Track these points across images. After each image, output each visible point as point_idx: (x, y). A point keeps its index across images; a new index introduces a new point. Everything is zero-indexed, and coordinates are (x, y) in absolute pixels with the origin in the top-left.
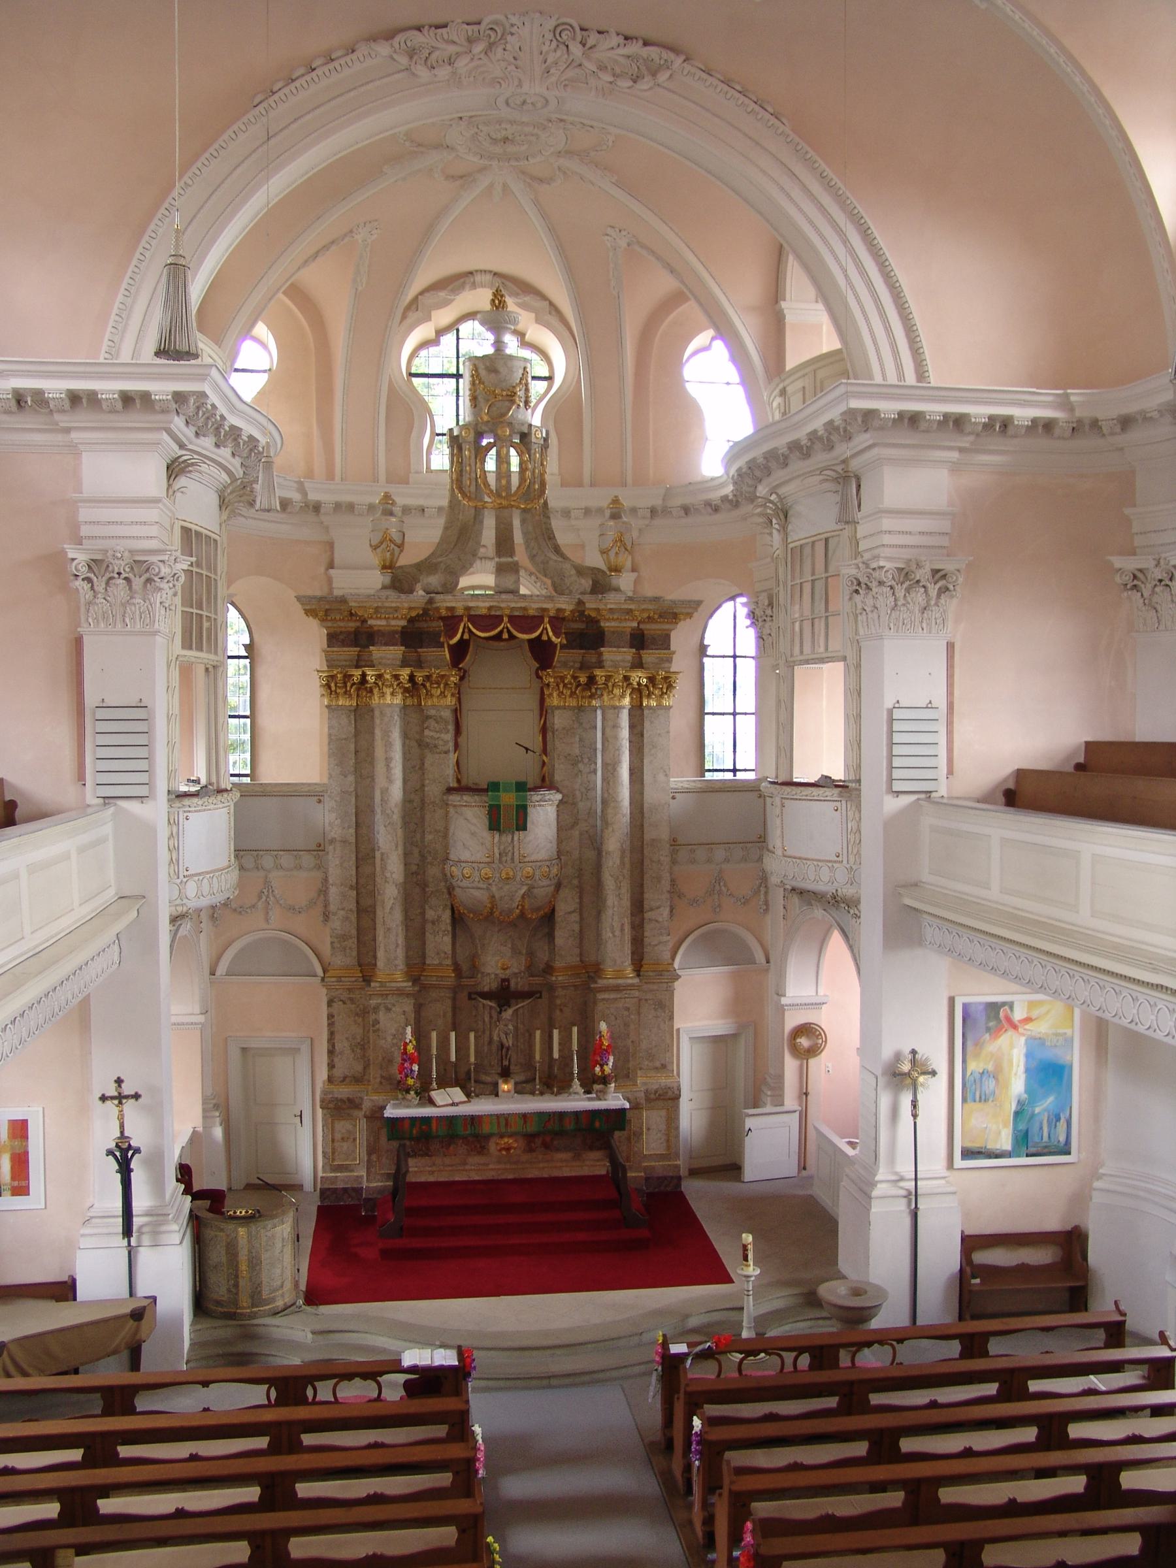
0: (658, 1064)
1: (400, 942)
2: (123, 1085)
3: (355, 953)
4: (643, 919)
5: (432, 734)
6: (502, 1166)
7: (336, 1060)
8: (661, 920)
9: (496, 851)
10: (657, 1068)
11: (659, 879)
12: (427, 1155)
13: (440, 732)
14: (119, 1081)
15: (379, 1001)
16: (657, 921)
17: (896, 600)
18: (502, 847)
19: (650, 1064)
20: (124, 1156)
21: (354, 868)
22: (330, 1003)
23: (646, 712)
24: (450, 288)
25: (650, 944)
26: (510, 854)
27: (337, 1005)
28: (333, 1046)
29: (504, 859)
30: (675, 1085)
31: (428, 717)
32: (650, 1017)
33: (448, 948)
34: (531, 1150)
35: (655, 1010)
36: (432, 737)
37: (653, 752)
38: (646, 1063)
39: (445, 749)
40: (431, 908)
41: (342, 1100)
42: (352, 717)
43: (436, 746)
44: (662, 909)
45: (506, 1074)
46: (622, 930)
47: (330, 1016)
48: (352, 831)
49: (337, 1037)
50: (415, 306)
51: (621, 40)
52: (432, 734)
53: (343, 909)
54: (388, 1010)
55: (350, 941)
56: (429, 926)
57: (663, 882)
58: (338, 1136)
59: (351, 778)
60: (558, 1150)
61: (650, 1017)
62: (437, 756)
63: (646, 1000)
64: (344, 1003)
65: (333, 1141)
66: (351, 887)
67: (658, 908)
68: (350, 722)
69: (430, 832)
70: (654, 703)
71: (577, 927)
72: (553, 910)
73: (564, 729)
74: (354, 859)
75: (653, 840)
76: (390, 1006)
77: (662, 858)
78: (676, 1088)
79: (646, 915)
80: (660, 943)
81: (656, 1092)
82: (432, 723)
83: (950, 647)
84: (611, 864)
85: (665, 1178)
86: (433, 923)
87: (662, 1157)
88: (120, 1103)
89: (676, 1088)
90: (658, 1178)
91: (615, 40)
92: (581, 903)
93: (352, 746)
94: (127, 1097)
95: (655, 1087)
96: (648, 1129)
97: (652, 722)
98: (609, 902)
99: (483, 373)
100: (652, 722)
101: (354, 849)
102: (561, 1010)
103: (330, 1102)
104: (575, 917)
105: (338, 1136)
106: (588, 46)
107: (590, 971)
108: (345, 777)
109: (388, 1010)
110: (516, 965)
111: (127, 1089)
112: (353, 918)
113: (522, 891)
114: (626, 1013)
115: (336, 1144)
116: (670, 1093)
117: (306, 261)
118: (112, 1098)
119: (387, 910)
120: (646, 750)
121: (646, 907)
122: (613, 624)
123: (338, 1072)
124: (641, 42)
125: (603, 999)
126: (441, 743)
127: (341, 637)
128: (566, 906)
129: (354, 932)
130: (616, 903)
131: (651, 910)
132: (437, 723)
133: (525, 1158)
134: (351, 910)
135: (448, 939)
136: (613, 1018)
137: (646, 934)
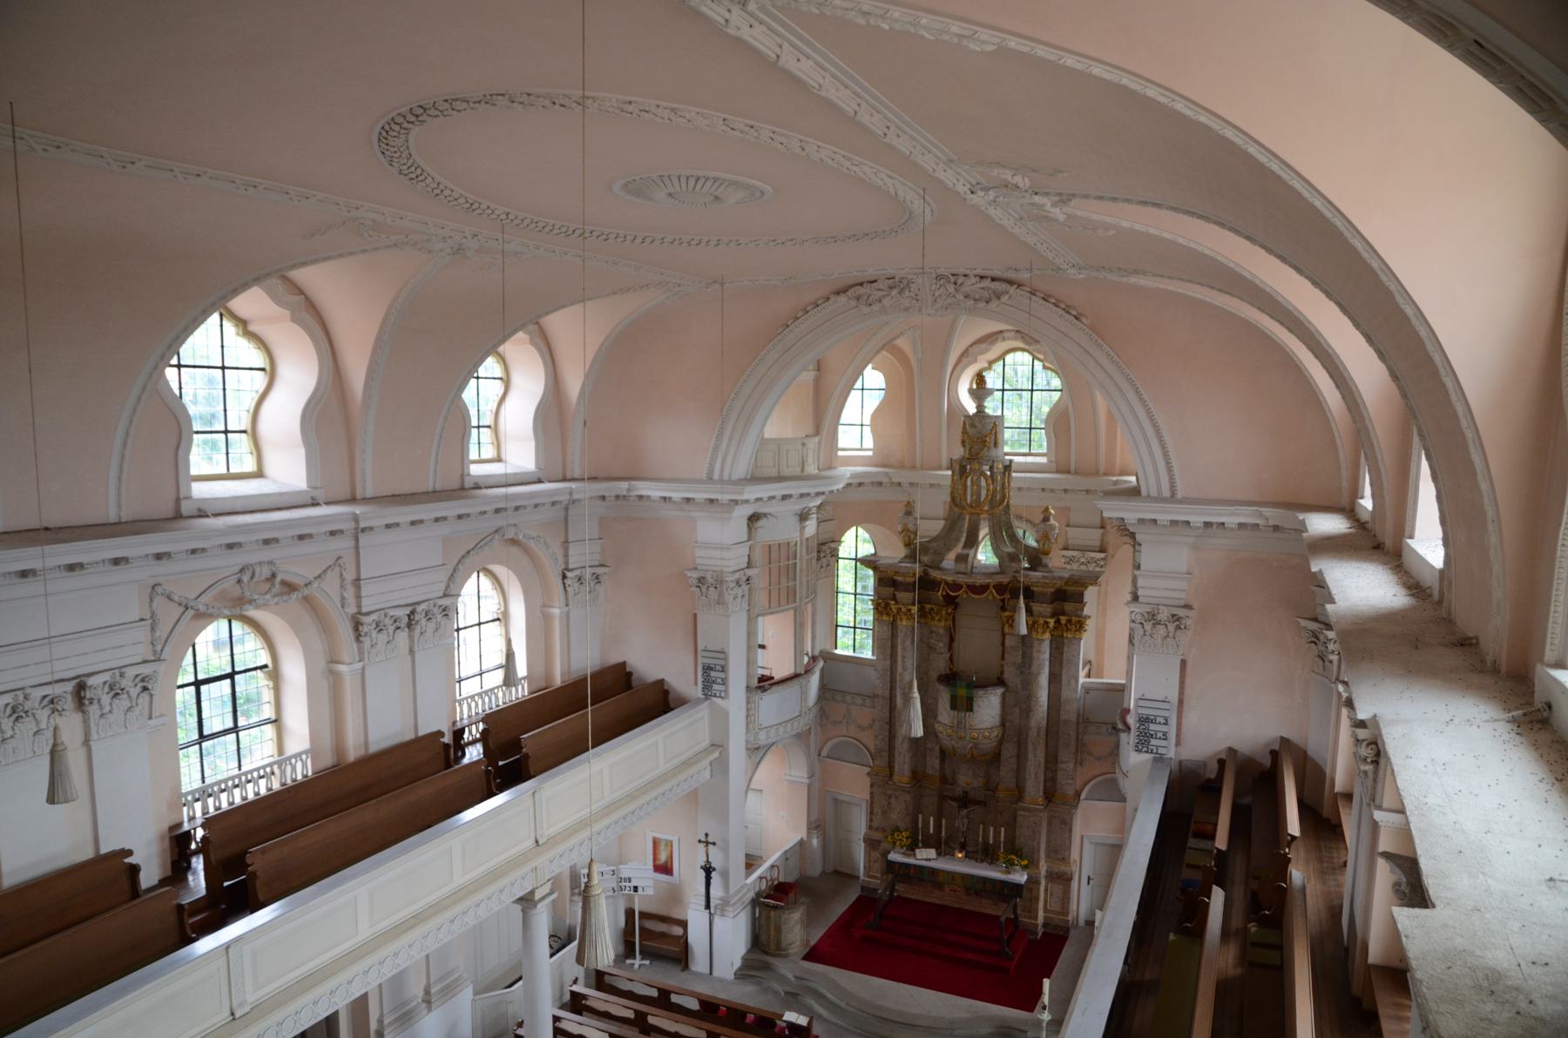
14: (707, 835)
16: (1066, 770)
22: (872, 786)
23: (1066, 640)
31: (932, 632)
33: (937, 766)
43: (936, 649)
45: (963, 847)
49: (875, 805)
50: (966, 355)
59: (888, 662)
66: (886, 723)
71: (1015, 766)
79: (1060, 766)
80: (1067, 783)
83: (1183, 663)
86: (930, 750)
91: (973, 280)
93: (889, 644)
104: (1014, 760)
109: (896, 798)
110: (978, 783)
111: (710, 840)
112: (887, 739)
120: (1065, 663)
123: (875, 825)
124: (989, 280)
128: (1009, 752)
129: (887, 748)
131: (1062, 763)
135: (937, 761)
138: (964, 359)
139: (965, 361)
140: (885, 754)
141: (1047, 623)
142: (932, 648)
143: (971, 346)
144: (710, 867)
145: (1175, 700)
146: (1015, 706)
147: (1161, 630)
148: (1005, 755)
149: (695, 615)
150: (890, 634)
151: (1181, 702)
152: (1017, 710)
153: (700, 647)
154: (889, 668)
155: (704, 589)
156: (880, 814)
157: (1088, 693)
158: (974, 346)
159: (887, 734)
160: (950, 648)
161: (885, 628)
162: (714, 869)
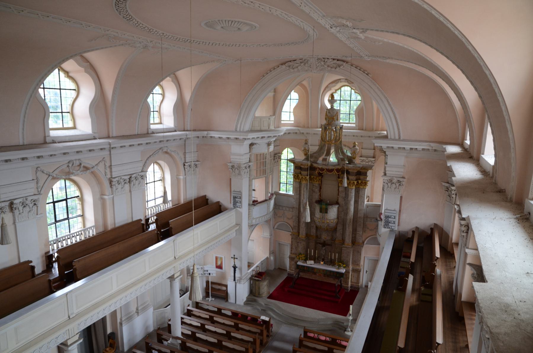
1: (304, 230)
7: (292, 250)
9: (321, 216)
13: (316, 189)
14: (234, 255)
17: (388, 186)
22: (292, 239)
45: (323, 260)
48: (298, 206)
50: (327, 87)
51: (332, 60)
59: (298, 196)
66: (297, 217)
70: (362, 187)
71: (342, 232)
72: (336, 228)
77: (361, 221)
83: (401, 197)
86: (313, 226)
91: (331, 60)
92: (343, 227)
99: (327, 113)
104: (341, 230)
105: (292, 264)
107: (343, 241)
112: (297, 223)
120: (360, 197)
121: (357, 231)
122: (351, 171)
123: (293, 252)
124: (336, 60)
128: (340, 228)
129: (297, 226)
131: (358, 231)
139: (327, 89)
140: (297, 228)
141: (354, 183)
142: (313, 191)
143: (329, 84)
144: (236, 266)
147: (394, 186)
148: (338, 228)
149: (231, 179)
151: (400, 211)
153: (232, 190)
158: (330, 84)
161: (297, 184)
162: (237, 267)
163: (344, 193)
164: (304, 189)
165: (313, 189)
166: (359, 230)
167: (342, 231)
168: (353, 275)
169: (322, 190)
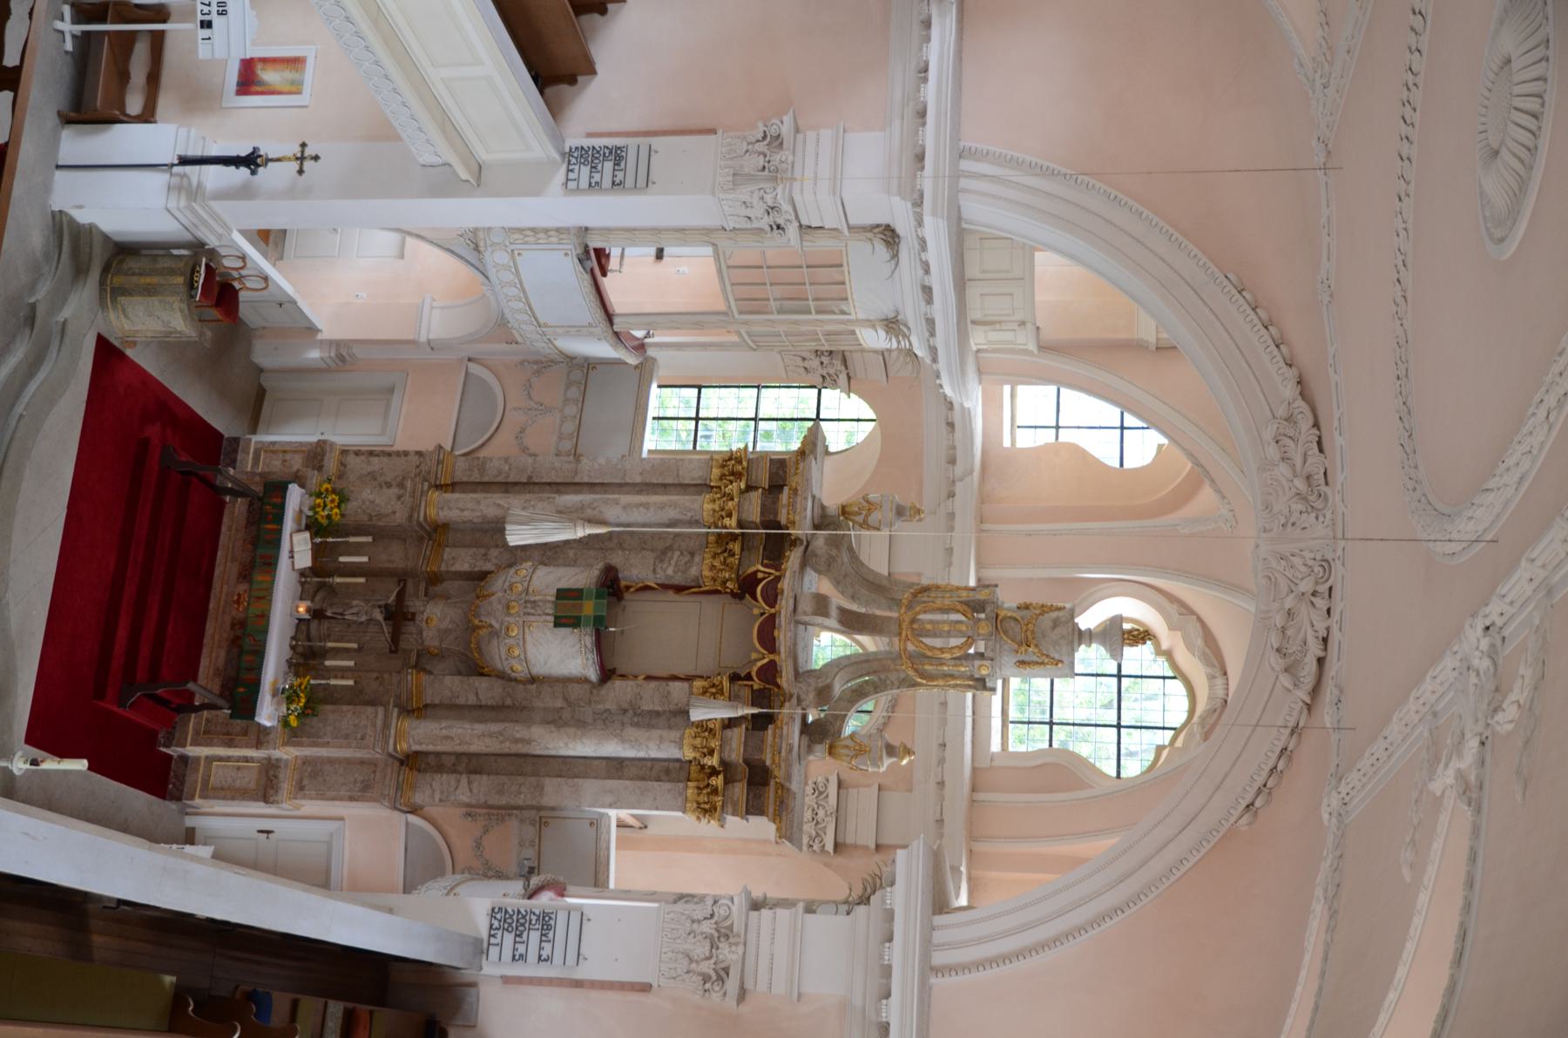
0: (305, 782)
1: (466, 513)
2: (313, 162)
3: (465, 479)
4: (461, 773)
5: (675, 558)
6: (223, 598)
7: (363, 458)
8: (458, 792)
9: (537, 598)
10: (301, 780)
11: (500, 792)
12: (248, 523)
13: (676, 565)
14: (316, 158)
15: (408, 489)
16: (457, 788)
18: (541, 604)
19: (306, 774)
20: (251, 161)
21: (549, 481)
22: (419, 454)
24: (1207, 650)
25: (433, 779)
26: (533, 611)
27: (415, 460)
28: (377, 455)
29: (529, 605)
30: (279, 798)
31: (692, 554)
32: (356, 775)
34: (233, 625)
35: (362, 782)
36: (672, 558)
37: (638, 791)
38: (309, 769)
39: (658, 570)
40: (501, 553)
41: (322, 460)
42: (699, 482)
43: (662, 561)
44: (469, 794)
45: (317, 614)
46: (447, 737)
47: (406, 454)
48: (586, 480)
49: (385, 459)
51: (1323, 633)
52: (675, 558)
53: (510, 469)
54: (399, 497)
55: (478, 476)
56: (483, 551)
57: (497, 797)
58: (288, 457)
59: (638, 479)
60: (228, 652)
61: (356, 775)
62: (652, 561)
63: (374, 772)
64: (417, 467)
65: (285, 452)
66: (530, 477)
67: (471, 791)
68: (694, 479)
69: (576, 554)
72: (482, 675)
73: (669, 693)
74: (558, 481)
75: (543, 788)
76: (403, 499)
77: (522, 796)
78: (276, 798)
81: (276, 777)
82: (687, 558)
83: (645, 988)
84: (516, 728)
85: (183, 783)
86: (485, 555)
87: (206, 782)
88: (297, 159)
89: (276, 798)
90: (184, 776)
91: (1321, 627)
94: (302, 164)
95: (281, 776)
96: (239, 768)
97: (669, 791)
98: (477, 726)
100: (669, 791)
101: (569, 480)
102: (377, 678)
103: (322, 449)
104: (472, 700)
105: (288, 457)
106: (1313, 599)
107: (416, 710)
108: (641, 474)
109: (399, 497)
111: (308, 165)
112: (501, 479)
113: (494, 623)
114: (359, 736)
115: (281, 455)
116: (272, 792)
117: (1192, 455)
118: (303, 152)
119: (497, 502)
120: (639, 783)
121: (473, 777)
124: (1322, 654)
125: (377, 713)
126: (665, 566)
127: (781, 472)
128: (485, 690)
129: (486, 479)
130: (475, 732)
131: (469, 783)
132: (686, 563)
133: (228, 620)
134: (508, 477)
135: (466, 567)
136: (356, 722)
137: (445, 776)
138: (1175, 606)
139: (1173, 609)
140: (476, 477)
141: (711, 752)
142: (663, 554)
143: (1199, 619)
144: (259, 166)
145: (581, 973)
146: (565, 699)
147: (702, 949)
148: (482, 684)
149: (713, 131)
150: (687, 482)
151: (578, 984)
152: (559, 703)
153: (656, 142)
154: (628, 480)
155: (761, 147)
156: (369, 469)
157: (591, 824)
158: (1198, 625)
159: (511, 479)
160: (665, 587)
162: (253, 173)
163: (658, 708)
164: (674, 505)
165: (677, 553)
166: (475, 785)
167: (470, 703)
168: (244, 767)
169: (671, 595)
